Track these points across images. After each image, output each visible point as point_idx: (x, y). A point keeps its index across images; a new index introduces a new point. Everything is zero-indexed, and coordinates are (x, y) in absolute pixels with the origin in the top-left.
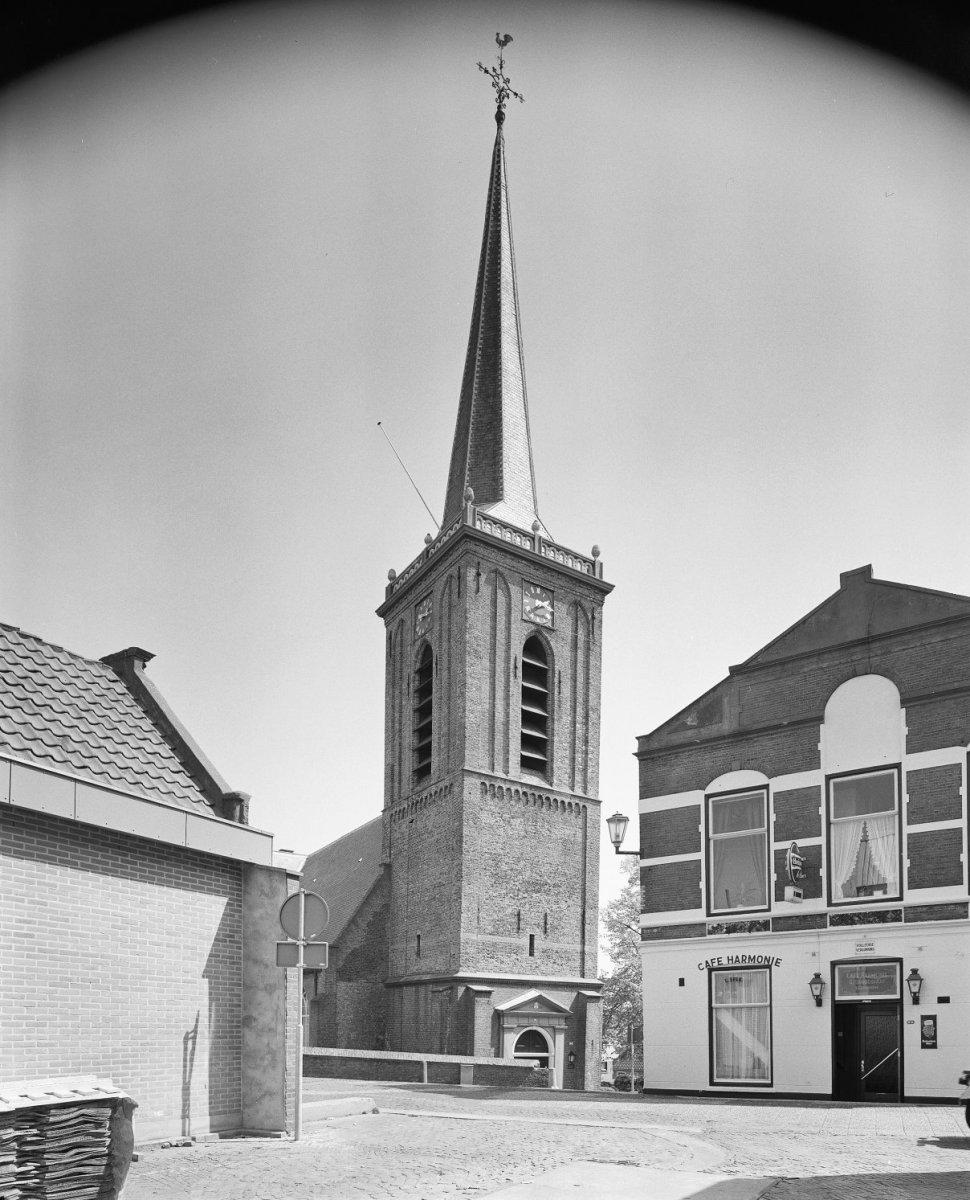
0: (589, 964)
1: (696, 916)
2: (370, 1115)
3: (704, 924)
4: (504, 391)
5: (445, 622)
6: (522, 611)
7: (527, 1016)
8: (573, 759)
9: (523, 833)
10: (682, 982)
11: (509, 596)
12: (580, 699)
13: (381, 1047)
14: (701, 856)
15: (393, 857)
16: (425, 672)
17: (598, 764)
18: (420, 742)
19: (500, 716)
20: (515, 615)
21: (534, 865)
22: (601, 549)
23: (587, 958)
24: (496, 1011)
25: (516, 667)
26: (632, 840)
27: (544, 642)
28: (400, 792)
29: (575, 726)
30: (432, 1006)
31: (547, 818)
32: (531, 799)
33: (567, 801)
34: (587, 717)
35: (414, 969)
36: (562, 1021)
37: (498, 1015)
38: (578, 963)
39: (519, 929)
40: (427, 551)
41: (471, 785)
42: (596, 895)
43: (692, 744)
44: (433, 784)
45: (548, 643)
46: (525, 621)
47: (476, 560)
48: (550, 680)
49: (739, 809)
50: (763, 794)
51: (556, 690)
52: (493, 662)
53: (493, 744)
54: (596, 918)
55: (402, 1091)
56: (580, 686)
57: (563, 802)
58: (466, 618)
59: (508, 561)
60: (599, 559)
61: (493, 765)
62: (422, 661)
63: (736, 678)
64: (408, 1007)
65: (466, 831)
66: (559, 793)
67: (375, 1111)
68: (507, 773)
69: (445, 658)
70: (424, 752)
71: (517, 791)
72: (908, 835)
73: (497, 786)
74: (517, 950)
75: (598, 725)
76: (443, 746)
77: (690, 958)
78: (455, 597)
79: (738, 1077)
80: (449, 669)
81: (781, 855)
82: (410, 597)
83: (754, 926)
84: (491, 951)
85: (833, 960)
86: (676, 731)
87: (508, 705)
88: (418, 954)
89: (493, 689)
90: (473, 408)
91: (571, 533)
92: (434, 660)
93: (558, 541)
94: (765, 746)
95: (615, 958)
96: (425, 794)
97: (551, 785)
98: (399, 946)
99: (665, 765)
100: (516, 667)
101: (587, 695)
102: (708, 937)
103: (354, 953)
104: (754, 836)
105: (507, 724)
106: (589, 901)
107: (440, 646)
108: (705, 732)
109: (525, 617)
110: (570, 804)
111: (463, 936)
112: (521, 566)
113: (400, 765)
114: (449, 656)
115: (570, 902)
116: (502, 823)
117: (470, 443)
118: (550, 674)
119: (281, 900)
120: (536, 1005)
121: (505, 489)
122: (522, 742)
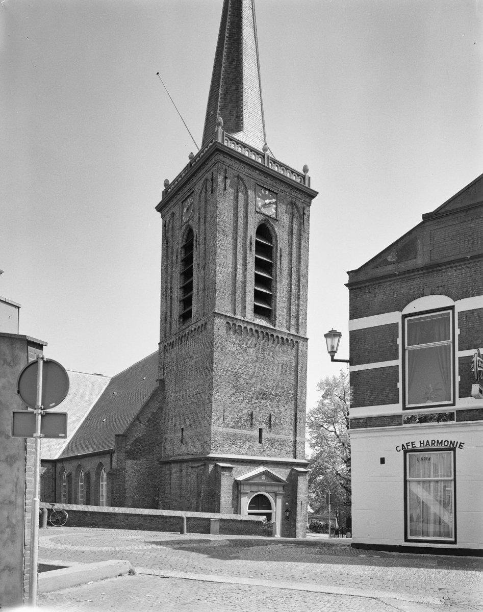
0: (299, 449)
1: (395, 409)
2: (126, 577)
3: (400, 416)
4: (244, 58)
5: (203, 212)
6: (256, 206)
7: (255, 484)
8: (290, 310)
9: (255, 358)
10: (383, 461)
11: (247, 195)
12: (294, 269)
13: (156, 507)
14: (398, 362)
15: (165, 375)
16: (188, 247)
17: (306, 313)
18: (184, 296)
19: (239, 277)
20: (251, 208)
21: (263, 381)
22: (309, 168)
23: (298, 445)
24: (236, 481)
25: (251, 244)
26: (344, 352)
27: (270, 228)
28: (171, 329)
29: (291, 287)
30: (192, 477)
31: (272, 349)
32: (260, 335)
33: (285, 337)
34: (299, 281)
35: (179, 452)
36: (281, 488)
37: (237, 484)
38: (291, 449)
39: (252, 424)
40: (190, 164)
41: (219, 323)
42: (304, 403)
43: (394, 275)
44: (192, 324)
45: (273, 228)
46: (258, 212)
47: (224, 167)
48: (274, 255)
49: (427, 327)
50: (449, 313)
51: (279, 261)
52: (235, 239)
53: (235, 296)
54: (304, 418)
55: (161, 547)
56: (294, 260)
57: (282, 338)
58: (217, 207)
59: (246, 170)
60: (308, 174)
61: (235, 310)
62: (187, 240)
63: (427, 224)
64: (175, 478)
65: (215, 356)
66: (280, 332)
67: (131, 572)
68: (244, 316)
69: (202, 237)
71: (251, 329)
72: (398, 403)
73: (237, 325)
74: (249, 439)
75: (306, 287)
76: (200, 297)
77: (389, 442)
78: (209, 193)
79: (428, 535)
80: (205, 244)
81: (466, 363)
82: (179, 197)
83: (441, 417)
84: (232, 439)
85: (385, 459)
86: (379, 266)
87: (245, 269)
88: (182, 441)
89: (235, 258)
90: (223, 69)
91: (290, 154)
92: (195, 238)
93: (278, 159)
94: (453, 275)
95: (313, 446)
96: (187, 331)
97: (275, 326)
98: (169, 436)
99: (369, 293)
100: (251, 244)
101: (299, 266)
102: (404, 426)
103: (138, 440)
104: (440, 347)
105: (244, 282)
106: (300, 407)
107: (199, 228)
108: (402, 266)
109: (258, 210)
110: (287, 339)
111: (213, 428)
112: (255, 174)
113: (171, 312)
114: (205, 234)
115: (287, 407)
117: (220, 92)
118: (274, 250)
119: (22, 367)
120: (264, 477)
121: (245, 123)
122: (255, 296)
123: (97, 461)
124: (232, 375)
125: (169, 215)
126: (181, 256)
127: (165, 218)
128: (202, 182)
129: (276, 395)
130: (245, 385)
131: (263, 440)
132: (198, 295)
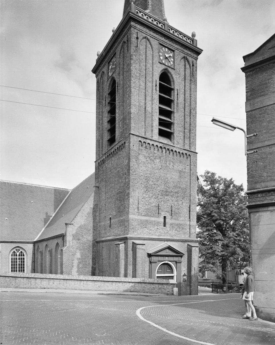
9: (160, 167)
16: (113, 94)
17: (195, 135)
22: (196, 34)
41: (134, 140)
60: (196, 38)
68: (152, 137)
70: (112, 131)
82: (106, 60)
84: (144, 224)
88: (110, 227)
100: (156, 86)
111: (131, 216)
116: (149, 161)
123: (55, 241)
124: (144, 179)
125: (100, 75)
126: (108, 100)
127: (98, 78)
128: (121, 44)
129: (175, 193)
130: (153, 186)
131: (167, 224)
132: (119, 125)
